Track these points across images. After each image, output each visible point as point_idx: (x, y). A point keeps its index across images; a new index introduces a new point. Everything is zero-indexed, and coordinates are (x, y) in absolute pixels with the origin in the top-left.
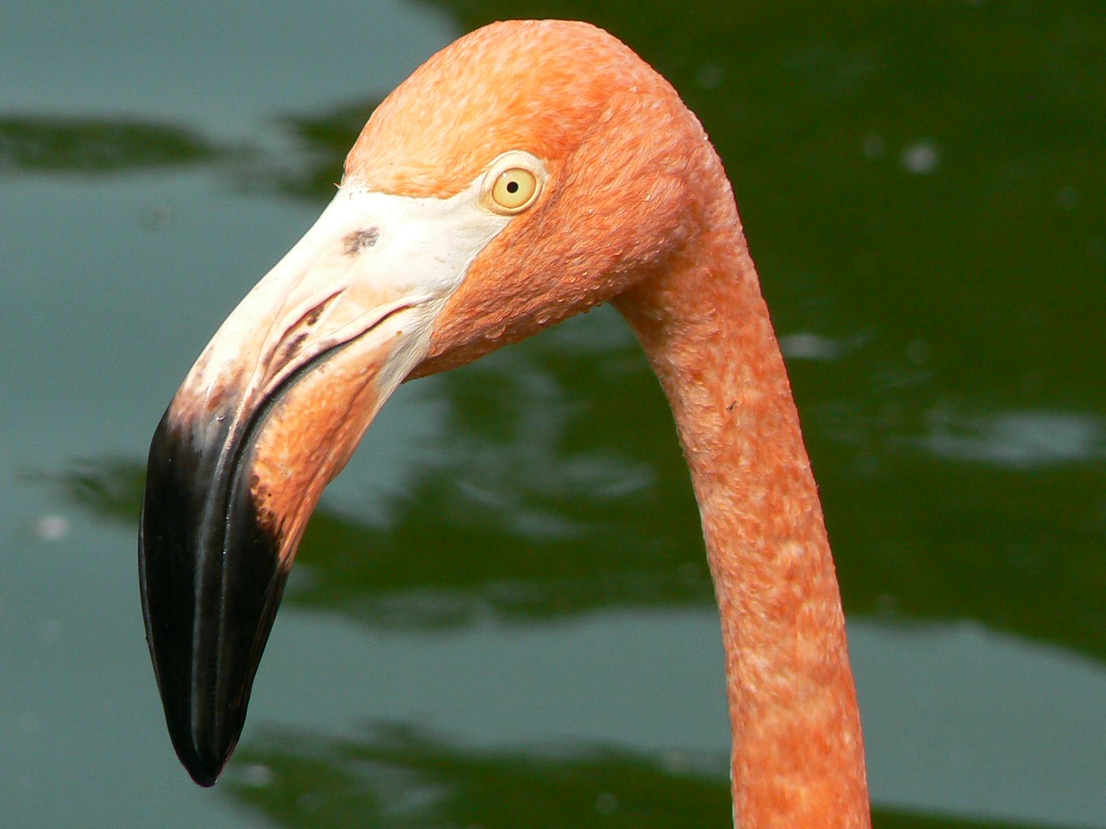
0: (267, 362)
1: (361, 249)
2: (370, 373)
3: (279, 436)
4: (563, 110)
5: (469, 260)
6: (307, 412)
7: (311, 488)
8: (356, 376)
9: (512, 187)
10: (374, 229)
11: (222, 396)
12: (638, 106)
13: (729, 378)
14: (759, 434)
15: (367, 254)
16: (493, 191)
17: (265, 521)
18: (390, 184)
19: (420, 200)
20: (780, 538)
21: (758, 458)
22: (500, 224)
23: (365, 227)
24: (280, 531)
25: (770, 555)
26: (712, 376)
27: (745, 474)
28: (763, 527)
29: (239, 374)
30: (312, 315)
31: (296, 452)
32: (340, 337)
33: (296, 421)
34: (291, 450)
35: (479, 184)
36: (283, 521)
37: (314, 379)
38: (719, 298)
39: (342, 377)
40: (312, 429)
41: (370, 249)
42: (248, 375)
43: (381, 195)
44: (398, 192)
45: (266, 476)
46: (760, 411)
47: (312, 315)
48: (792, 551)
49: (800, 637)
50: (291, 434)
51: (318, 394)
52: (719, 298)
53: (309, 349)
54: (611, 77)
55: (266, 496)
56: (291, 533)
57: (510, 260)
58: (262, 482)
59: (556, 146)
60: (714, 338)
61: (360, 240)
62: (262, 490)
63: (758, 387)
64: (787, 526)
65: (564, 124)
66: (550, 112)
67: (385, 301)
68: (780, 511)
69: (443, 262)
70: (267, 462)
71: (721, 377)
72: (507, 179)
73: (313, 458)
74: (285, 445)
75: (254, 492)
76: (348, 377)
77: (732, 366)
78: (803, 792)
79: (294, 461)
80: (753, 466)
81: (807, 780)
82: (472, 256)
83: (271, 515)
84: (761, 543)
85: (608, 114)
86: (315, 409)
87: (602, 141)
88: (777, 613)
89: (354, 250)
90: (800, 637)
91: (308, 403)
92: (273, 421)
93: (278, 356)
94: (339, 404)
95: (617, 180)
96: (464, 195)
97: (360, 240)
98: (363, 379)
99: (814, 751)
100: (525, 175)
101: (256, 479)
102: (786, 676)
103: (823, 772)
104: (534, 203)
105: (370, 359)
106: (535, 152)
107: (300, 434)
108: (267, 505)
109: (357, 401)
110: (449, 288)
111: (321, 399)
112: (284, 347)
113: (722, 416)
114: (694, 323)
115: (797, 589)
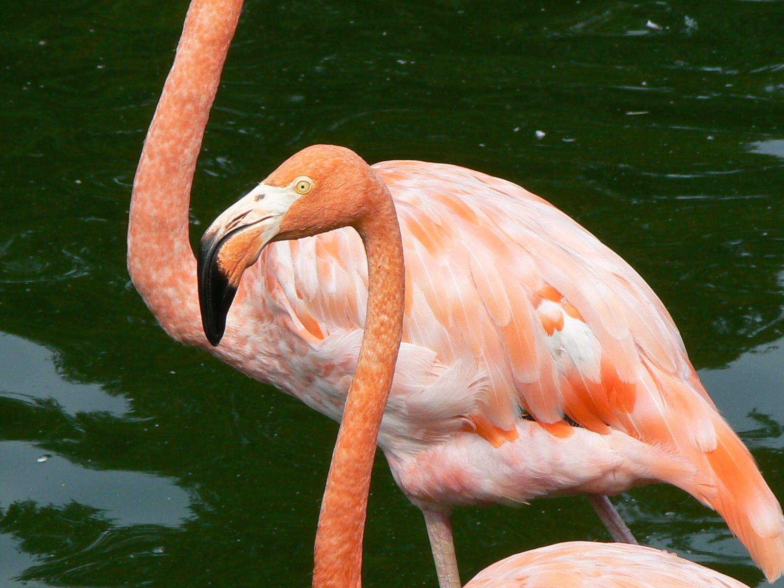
0: (227, 227)
1: (260, 199)
2: (258, 233)
3: (226, 247)
4: (322, 166)
5: (290, 205)
6: (235, 242)
7: (240, 264)
8: (252, 234)
9: (303, 187)
10: (264, 194)
11: (214, 234)
12: (349, 170)
13: (381, 259)
14: (386, 279)
15: (261, 201)
16: (297, 186)
17: (221, 270)
18: (270, 184)
19: (276, 188)
20: (383, 311)
21: (383, 286)
22: (299, 196)
23: (262, 194)
24: (227, 274)
25: (378, 315)
26: (376, 256)
27: (378, 289)
28: (379, 305)
29: (219, 229)
30: (243, 216)
31: (232, 252)
32: (249, 223)
33: (232, 244)
34: (230, 252)
35: (292, 184)
36: (228, 272)
37: (240, 233)
38: (382, 234)
39: (248, 234)
40: (238, 247)
41: (262, 200)
42: (220, 230)
43: (267, 186)
44: (271, 185)
45: (221, 258)
46: (388, 273)
47: (243, 216)
48: (385, 318)
49: (378, 344)
50: (230, 247)
51: (240, 237)
52: (382, 234)
53: (240, 225)
54: (342, 161)
55: (221, 264)
56: (233, 276)
57: (302, 208)
58: (220, 259)
59: (318, 177)
60: (379, 246)
61: (261, 197)
62: (220, 261)
63: (389, 265)
64: (386, 310)
65: (322, 171)
66: (317, 167)
67: (264, 214)
68: (386, 304)
69: (281, 205)
70: (222, 254)
71: (379, 257)
72: (303, 184)
73: (239, 255)
74: (228, 250)
75: (217, 262)
76: (250, 233)
77: (383, 255)
78: (363, 387)
79: (232, 255)
80: (382, 287)
81: (364, 385)
82: (291, 204)
83: (223, 269)
84: (377, 310)
85: (337, 171)
86: (238, 241)
87: (335, 178)
88: (374, 333)
89: (258, 200)
90: (378, 344)
91: (236, 239)
92: (225, 243)
93: (231, 226)
94: (248, 241)
95: (339, 190)
96: (289, 187)
97: (261, 197)
98: (255, 235)
99: (370, 377)
100: (306, 183)
101: (219, 258)
102: (371, 352)
103: (369, 385)
104: (310, 191)
105: (257, 230)
106: (309, 177)
107: (233, 248)
108: (222, 266)
109: (254, 241)
110: (283, 213)
111: (241, 238)
112: (234, 223)
113: (376, 269)
114: (373, 239)
115: (383, 329)
